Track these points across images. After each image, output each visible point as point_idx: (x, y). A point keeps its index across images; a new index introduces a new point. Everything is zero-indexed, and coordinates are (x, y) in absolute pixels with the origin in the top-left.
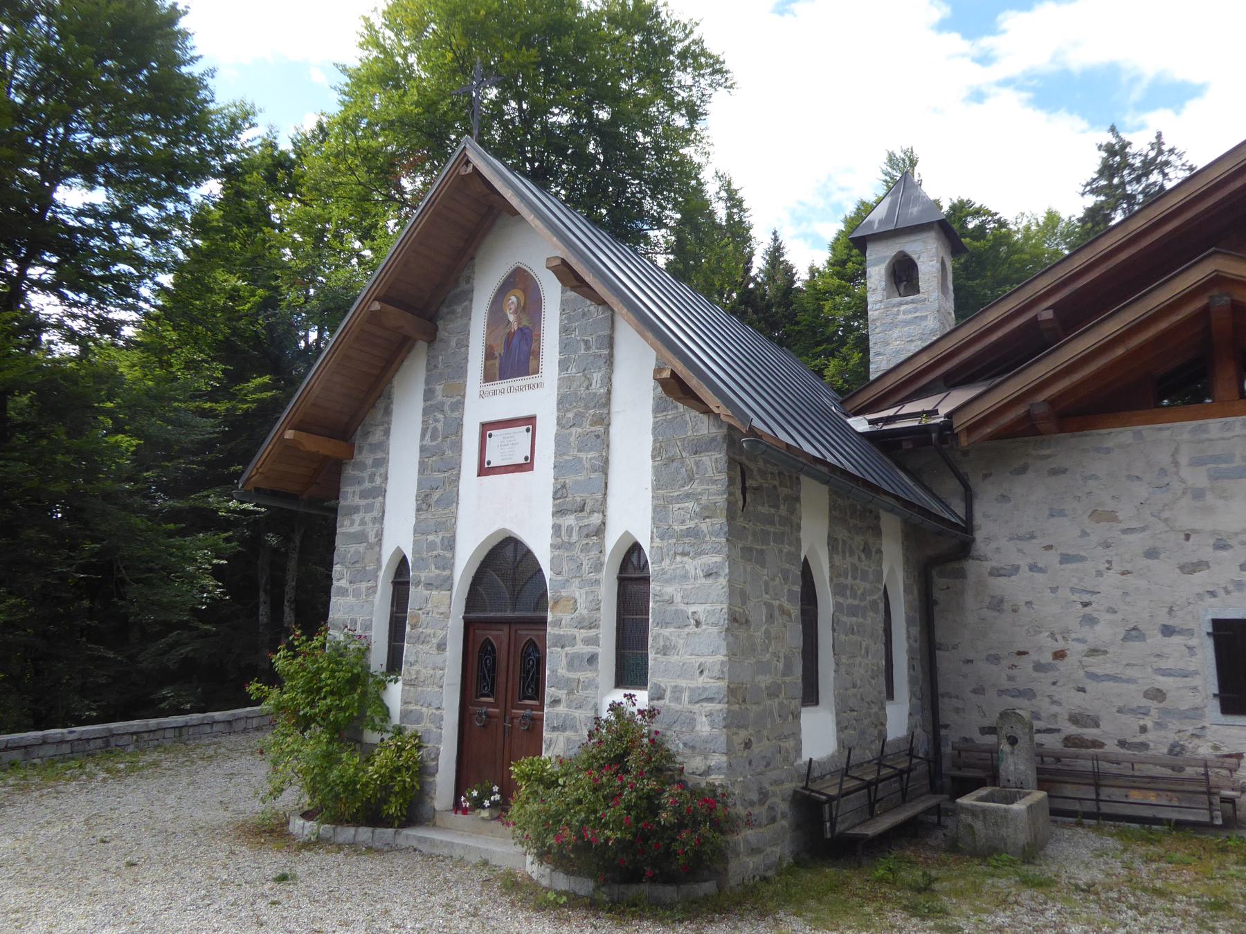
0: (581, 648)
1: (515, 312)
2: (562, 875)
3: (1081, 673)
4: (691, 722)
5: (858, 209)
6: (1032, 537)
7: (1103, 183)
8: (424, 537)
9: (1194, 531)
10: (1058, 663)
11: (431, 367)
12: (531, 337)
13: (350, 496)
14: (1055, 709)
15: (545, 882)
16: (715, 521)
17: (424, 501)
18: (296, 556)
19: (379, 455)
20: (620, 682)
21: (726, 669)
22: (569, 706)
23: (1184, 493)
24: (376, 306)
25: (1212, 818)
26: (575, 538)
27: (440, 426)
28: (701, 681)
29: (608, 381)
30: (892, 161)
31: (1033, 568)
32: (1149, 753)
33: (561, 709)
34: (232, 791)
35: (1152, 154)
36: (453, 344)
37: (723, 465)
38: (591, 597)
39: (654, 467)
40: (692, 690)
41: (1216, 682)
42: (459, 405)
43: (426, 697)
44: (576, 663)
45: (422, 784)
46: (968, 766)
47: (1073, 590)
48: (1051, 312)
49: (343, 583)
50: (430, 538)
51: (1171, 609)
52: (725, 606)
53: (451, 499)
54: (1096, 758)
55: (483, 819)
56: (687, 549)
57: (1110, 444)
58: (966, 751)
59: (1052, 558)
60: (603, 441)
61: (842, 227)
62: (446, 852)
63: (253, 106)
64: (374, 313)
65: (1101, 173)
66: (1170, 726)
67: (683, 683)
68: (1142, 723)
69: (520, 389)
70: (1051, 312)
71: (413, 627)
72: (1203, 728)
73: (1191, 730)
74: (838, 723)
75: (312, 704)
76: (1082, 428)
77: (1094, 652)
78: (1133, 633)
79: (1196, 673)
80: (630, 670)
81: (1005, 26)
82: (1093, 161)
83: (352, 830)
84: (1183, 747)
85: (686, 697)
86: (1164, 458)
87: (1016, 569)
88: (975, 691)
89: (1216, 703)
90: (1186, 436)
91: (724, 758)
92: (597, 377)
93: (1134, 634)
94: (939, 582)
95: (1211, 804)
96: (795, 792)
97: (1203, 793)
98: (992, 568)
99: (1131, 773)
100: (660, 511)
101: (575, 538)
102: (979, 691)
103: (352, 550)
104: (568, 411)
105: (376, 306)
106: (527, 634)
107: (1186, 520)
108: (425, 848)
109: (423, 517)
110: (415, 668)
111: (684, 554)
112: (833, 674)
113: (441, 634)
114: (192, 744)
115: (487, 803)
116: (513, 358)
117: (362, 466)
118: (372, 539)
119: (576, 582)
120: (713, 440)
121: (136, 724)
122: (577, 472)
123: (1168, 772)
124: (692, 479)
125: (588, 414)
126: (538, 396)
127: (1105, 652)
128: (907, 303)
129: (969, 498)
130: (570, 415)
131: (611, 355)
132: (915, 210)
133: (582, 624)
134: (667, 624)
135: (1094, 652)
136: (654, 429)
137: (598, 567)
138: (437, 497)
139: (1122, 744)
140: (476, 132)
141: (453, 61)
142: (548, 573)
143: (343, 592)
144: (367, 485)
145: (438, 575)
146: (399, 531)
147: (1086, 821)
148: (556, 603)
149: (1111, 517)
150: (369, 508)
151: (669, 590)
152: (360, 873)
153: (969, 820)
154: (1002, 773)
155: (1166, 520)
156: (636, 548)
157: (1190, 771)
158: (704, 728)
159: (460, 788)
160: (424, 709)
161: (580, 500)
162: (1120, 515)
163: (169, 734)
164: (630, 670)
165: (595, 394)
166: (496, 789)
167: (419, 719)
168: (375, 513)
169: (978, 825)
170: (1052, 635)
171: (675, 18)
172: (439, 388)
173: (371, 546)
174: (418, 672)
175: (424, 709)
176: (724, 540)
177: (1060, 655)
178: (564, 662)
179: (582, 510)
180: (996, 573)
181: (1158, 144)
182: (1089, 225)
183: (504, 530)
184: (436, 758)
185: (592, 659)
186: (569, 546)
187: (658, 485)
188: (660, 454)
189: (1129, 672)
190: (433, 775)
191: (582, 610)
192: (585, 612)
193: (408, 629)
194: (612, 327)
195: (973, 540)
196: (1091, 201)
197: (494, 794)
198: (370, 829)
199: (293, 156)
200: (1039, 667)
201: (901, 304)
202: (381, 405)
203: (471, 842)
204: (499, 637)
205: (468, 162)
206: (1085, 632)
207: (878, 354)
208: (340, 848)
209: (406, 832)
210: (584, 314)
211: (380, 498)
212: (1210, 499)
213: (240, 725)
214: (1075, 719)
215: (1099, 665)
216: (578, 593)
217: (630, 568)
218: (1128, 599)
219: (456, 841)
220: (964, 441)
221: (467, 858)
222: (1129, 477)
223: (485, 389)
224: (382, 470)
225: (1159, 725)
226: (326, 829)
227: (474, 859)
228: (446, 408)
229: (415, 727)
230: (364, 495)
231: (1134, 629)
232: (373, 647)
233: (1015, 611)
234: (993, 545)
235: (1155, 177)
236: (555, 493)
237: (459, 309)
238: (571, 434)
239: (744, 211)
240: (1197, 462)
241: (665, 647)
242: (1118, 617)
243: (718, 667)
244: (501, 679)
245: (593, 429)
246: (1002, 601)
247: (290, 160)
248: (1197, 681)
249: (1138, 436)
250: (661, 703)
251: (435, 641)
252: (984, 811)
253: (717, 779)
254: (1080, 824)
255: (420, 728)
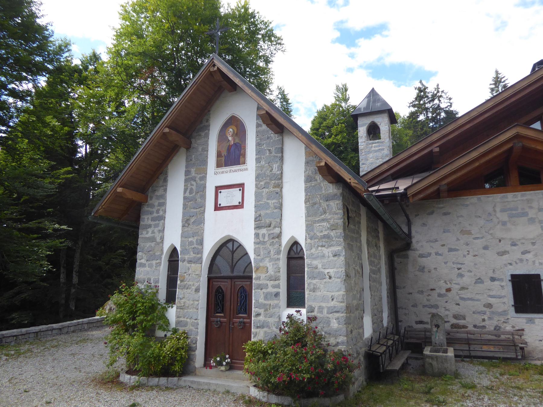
0: (271, 290)
1: (232, 136)
2: (274, 396)
3: (458, 297)
4: (328, 323)
5: (323, 108)
6: (436, 241)
7: (417, 103)
8: (187, 239)
9: (502, 238)
10: (448, 293)
11: (188, 160)
12: (241, 147)
13: (145, 220)
14: (447, 313)
15: (264, 400)
16: (337, 231)
17: (186, 223)
18: (79, 251)
19: (162, 201)
20: (290, 305)
21: (345, 298)
22: (265, 317)
23: (498, 223)
24: (167, 130)
25: (517, 356)
26: (266, 239)
27: (194, 188)
28: (332, 304)
29: (281, 168)
30: (338, 88)
31: (437, 254)
32: (486, 330)
33: (261, 318)
34: (78, 362)
35: (435, 92)
36: (200, 150)
37: (341, 206)
38: (275, 266)
39: (306, 207)
40: (328, 308)
41: (513, 300)
42: (204, 178)
43: (189, 314)
44: (269, 297)
45: (189, 356)
46: (411, 338)
47: (453, 263)
48: (438, 148)
49: (143, 261)
50: (190, 239)
51: (494, 270)
52: (343, 269)
53: (201, 221)
54: (467, 333)
55: (222, 371)
56: (324, 244)
57: (468, 203)
58: (410, 331)
59: (445, 250)
60: (279, 195)
61: (316, 115)
62: (206, 387)
63: (70, 41)
64: (164, 134)
65: (416, 99)
66: (495, 318)
67: (324, 305)
68: (483, 317)
69: (236, 171)
70: (438, 148)
71: (181, 281)
72: (508, 319)
73: (503, 320)
74: (372, 321)
75: (134, 319)
76: (456, 196)
77: (463, 288)
78: (479, 280)
79: (505, 296)
80: (295, 298)
81: (359, 44)
82: (414, 94)
83: (156, 379)
84: (500, 327)
85: (325, 311)
86: (490, 209)
87: (429, 254)
88: (413, 306)
89: (513, 309)
90: (498, 200)
91: (345, 338)
92: (275, 166)
93: (479, 281)
94: (397, 260)
95: (516, 350)
96: (366, 352)
97: (513, 346)
98: (420, 254)
99: (480, 338)
100: (309, 227)
101: (266, 239)
102: (415, 306)
103: (148, 245)
104: (261, 181)
105: (167, 130)
106: (239, 283)
107: (499, 234)
108: (195, 386)
109: (186, 230)
110: (183, 300)
111: (322, 246)
112: (370, 300)
113: (197, 284)
114: (43, 340)
115: (224, 363)
116: (232, 156)
117: (153, 206)
118: (158, 240)
119: (267, 259)
120: (336, 195)
121: (15, 331)
122: (267, 209)
123: (494, 338)
124: (325, 212)
125: (271, 184)
126: (247, 174)
127: (467, 289)
128: (375, 143)
129: (409, 224)
130: (262, 183)
131: (282, 156)
132: (379, 104)
133: (270, 279)
134: (315, 278)
135: (463, 288)
136: (306, 190)
137: (278, 252)
138: (193, 219)
139: (475, 326)
140: (217, 52)
141: (168, 28)
142: (252, 256)
143: (143, 265)
144: (155, 215)
145: (195, 257)
146: (173, 235)
147: (465, 359)
148: (257, 269)
149: (469, 233)
150: (156, 226)
151: (315, 262)
152: (170, 400)
153: (430, 361)
154: (433, 340)
155: (491, 234)
156: (296, 243)
157: (503, 337)
158: (335, 325)
159: (207, 356)
160: (188, 320)
161: (268, 221)
162: (473, 232)
163: (32, 336)
164: (295, 298)
165: (275, 174)
166: (227, 356)
167: (186, 324)
168: (160, 228)
169: (434, 363)
170: (445, 282)
171: (262, 19)
172: (193, 170)
173: (158, 244)
174: (184, 303)
175: (188, 320)
176: (342, 240)
177: (449, 290)
178: (262, 296)
179: (270, 226)
180: (421, 256)
181: (437, 89)
182: (411, 119)
183: (229, 235)
184: (196, 343)
185: (277, 295)
186: (264, 243)
187: (308, 215)
188: (309, 201)
189: (478, 297)
190: (195, 351)
191: (271, 272)
192: (272, 273)
193: (178, 282)
194: (283, 144)
195: (412, 242)
196: (413, 109)
197: (227, 359)
198: (166, 378)
199: (81, 67)
200: (440, 295)
201: (373, 143)
202: (162, 177)
203: (219, 382)
204: (225, 285)
205: (214, 65)
206: (459, 280)
207: (363, 164)
208: (152, 388)
209: (184, 378)
210: (268, 138)
211: (162, 221)
212: (509, 225)
213: (66, 330)
214: (455, 317)
215: (465, 294)
216: (267, 263)
217: (292, 252)
218: (476, 266)
219: (195, 380)
220: (411, 200)
221: (218, 390)
222: (476, 216)
223: (217, 171)
224: (163, 208)
225: (490, 318)
226: (143, 379)
227: (222, 390)
228: (197, 179)
229: (183, 328)
230: (153, 219)
231: (479, 279)
232: (160, 291)
233: (429, 272)
234: (420, 244)
235: (436, 101)
236: (256, 219)
237: (203, 134)
238: (263, 192)
239: (290, 104)
240: (503, 211)
241: (314, 288)
242: (472, 274)
243: (341, 297)
244: (227, 304)
245: (274, 189)
246: (424, 268)
247: (80, 69)
248: (505, 300)
249: (479, 199)
250: (313, 314)
251: (194, 288)
252: (437, 357)
253: (342, 348)
254: (463, 361)
255: (186, 329)
